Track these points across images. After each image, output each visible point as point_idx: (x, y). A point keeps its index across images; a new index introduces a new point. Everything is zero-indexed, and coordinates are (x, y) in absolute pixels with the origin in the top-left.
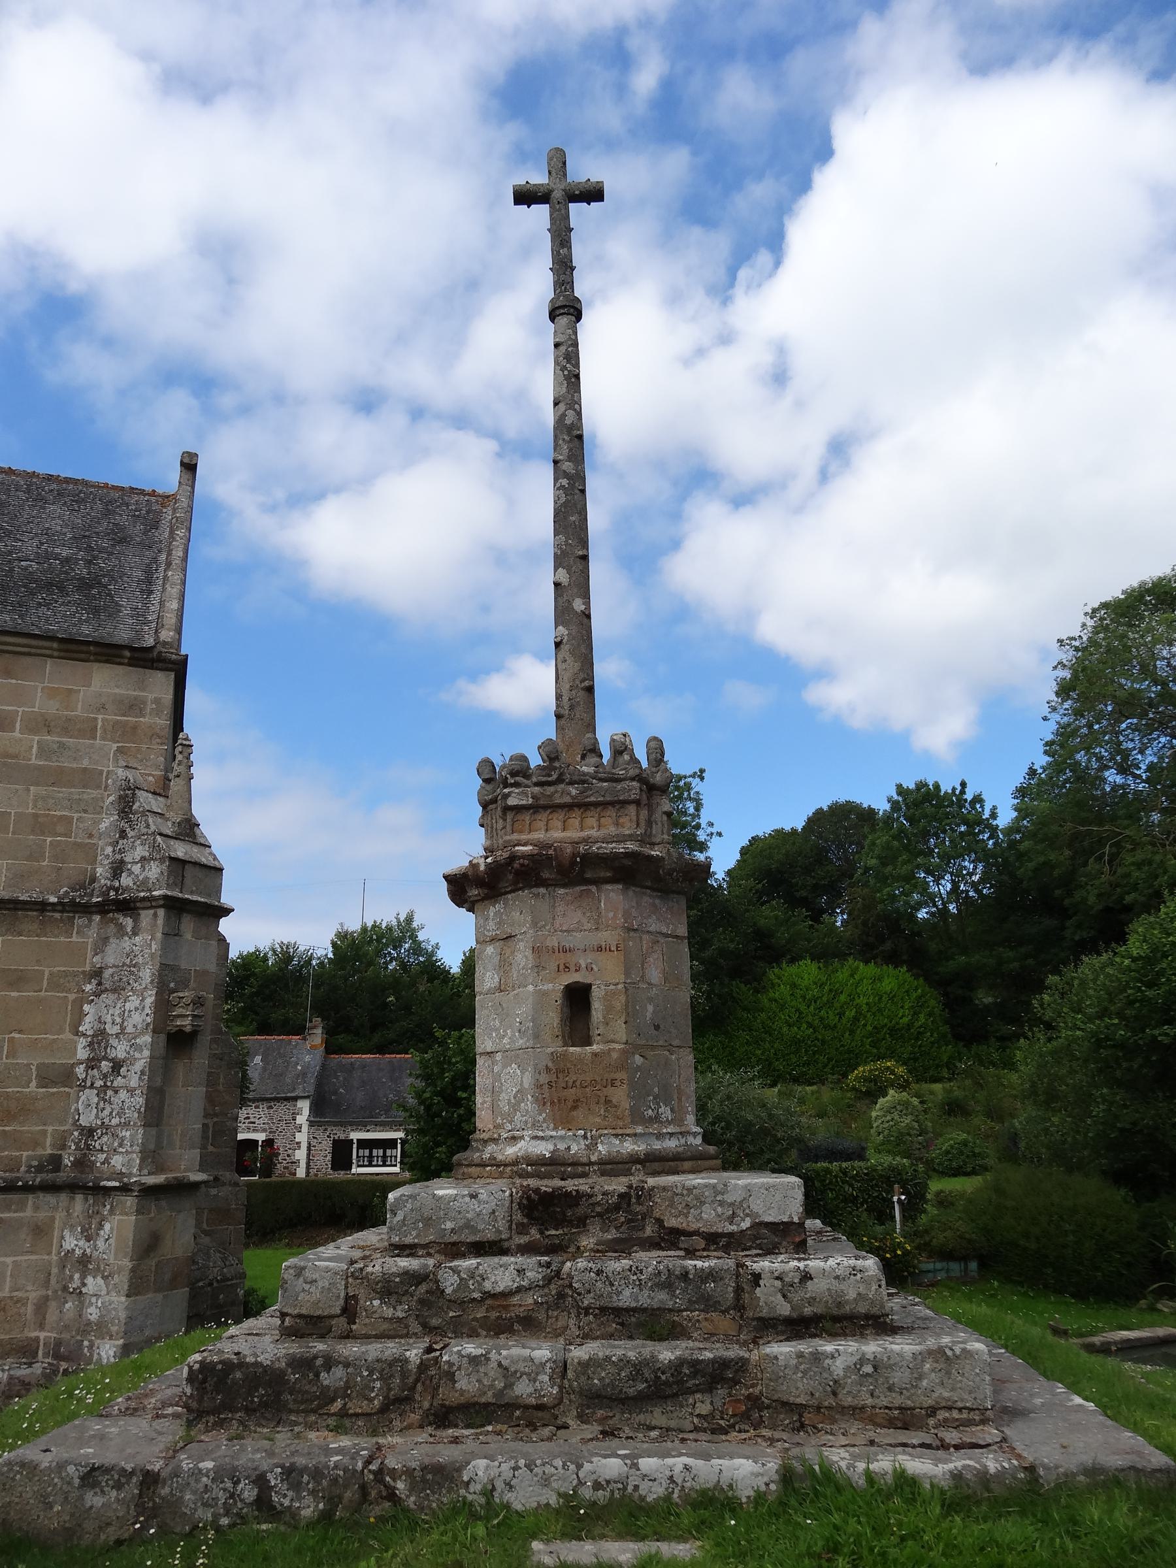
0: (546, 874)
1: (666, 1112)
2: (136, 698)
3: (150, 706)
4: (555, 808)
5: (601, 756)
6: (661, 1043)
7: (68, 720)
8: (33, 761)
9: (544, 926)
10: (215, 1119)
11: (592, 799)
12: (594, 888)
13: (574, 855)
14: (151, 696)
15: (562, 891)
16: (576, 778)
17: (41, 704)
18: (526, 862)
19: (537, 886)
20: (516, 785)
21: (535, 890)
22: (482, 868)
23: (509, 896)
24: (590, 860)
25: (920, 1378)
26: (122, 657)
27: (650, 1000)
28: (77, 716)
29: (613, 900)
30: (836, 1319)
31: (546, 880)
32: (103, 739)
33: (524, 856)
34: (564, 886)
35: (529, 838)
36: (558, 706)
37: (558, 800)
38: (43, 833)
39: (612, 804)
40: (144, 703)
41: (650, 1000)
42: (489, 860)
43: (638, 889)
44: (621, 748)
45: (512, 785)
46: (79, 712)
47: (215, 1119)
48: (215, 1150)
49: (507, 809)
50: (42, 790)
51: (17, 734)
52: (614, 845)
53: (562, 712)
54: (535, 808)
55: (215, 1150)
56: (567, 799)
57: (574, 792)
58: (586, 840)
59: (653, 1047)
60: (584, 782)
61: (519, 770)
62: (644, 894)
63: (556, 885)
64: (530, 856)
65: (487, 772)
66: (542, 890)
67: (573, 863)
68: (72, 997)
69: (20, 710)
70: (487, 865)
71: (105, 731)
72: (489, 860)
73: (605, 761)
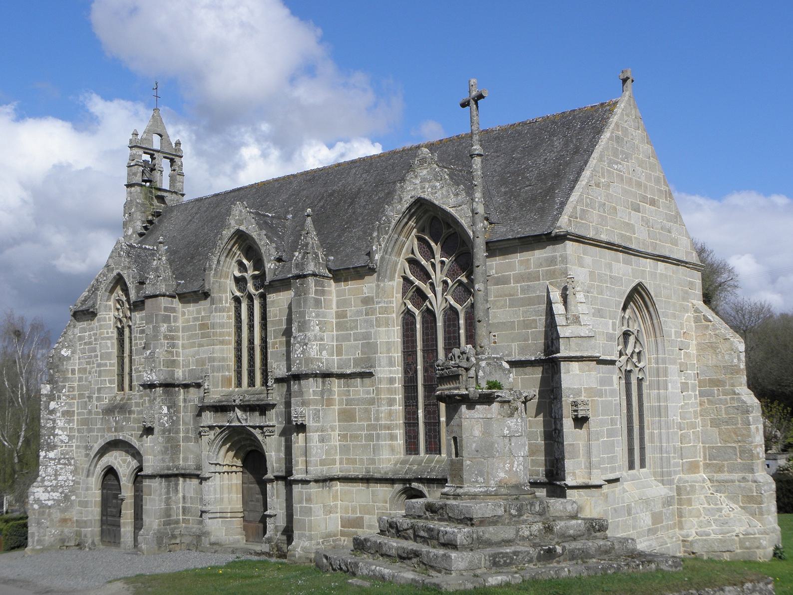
1: (481, 479)
2: (553, 256)
3: (559, 259)
6: (479, 456)
7: (529, 274)
8: (519, 296)
10: (739, 444)
14: (558, 254)
17: (519, 270)
26: (543, 239)
27: (474, 442)
28: (532, 271)
29: (158, 480)
30: (451, 545)
32: (543, 280)
38: (528, 329)
40: (556, 258)
41: (474, 442)
46: (532, 269)
47: (739, 444)
48: (741, 461)
50: (525, 308)
51: (512, 285)
55: (741, 461)
59: (475, 458)
65: (640, 284)
68: (548, 401)
69: (512, 273)
71: (543, 276)
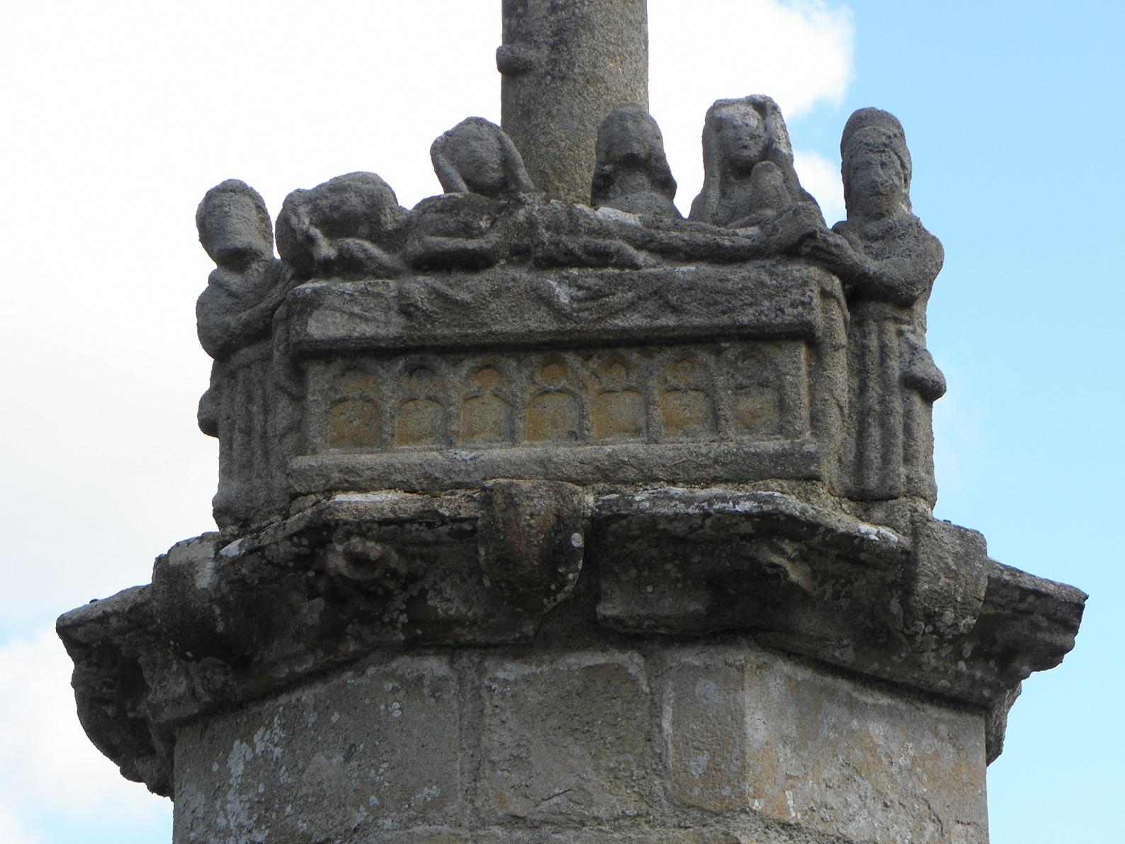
0: (448, 602)
4: (493, 351)
5: (667, 185)
9: (438, 803)
11: (634, 320)
12: (632, 662)
13: (562, 524)
15: (510, 670)
16: (575, 244)
18: (374, 549)
19: (413, 646)
20: (348, 266)
21: (405, 665)
22: (205, 578)
23: (306, 695)
24: (615, 543)
25: (94, 688)
31: (449, 624)
33: (362, 526)
34: (521, 650)
35: (380, 467)
36: (510, 34)
37: (506, 325)
39: (711, 339)
42: (233, 549)
43: (803, 674)
44: (745, 146)
45: (327, 269)
49: (309, 355)
52: (716, 490)
53: (531, 54)
54: (417, 353)
56: (538, 322)
57: (563, 295)
58: (608, 474)
60: (600, 258)
61: (348, 209)
62: (832, 694)
63: (487, 648)
64: (390, 527)
66: (434, 666)
67: (557, 552)
70: (225, 568)
72: (233, 549)
73: (684, 202)
